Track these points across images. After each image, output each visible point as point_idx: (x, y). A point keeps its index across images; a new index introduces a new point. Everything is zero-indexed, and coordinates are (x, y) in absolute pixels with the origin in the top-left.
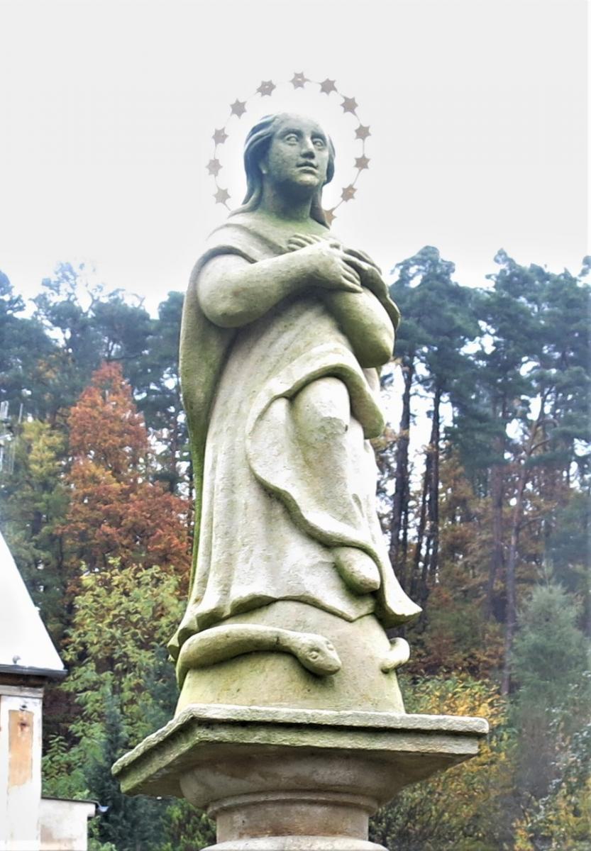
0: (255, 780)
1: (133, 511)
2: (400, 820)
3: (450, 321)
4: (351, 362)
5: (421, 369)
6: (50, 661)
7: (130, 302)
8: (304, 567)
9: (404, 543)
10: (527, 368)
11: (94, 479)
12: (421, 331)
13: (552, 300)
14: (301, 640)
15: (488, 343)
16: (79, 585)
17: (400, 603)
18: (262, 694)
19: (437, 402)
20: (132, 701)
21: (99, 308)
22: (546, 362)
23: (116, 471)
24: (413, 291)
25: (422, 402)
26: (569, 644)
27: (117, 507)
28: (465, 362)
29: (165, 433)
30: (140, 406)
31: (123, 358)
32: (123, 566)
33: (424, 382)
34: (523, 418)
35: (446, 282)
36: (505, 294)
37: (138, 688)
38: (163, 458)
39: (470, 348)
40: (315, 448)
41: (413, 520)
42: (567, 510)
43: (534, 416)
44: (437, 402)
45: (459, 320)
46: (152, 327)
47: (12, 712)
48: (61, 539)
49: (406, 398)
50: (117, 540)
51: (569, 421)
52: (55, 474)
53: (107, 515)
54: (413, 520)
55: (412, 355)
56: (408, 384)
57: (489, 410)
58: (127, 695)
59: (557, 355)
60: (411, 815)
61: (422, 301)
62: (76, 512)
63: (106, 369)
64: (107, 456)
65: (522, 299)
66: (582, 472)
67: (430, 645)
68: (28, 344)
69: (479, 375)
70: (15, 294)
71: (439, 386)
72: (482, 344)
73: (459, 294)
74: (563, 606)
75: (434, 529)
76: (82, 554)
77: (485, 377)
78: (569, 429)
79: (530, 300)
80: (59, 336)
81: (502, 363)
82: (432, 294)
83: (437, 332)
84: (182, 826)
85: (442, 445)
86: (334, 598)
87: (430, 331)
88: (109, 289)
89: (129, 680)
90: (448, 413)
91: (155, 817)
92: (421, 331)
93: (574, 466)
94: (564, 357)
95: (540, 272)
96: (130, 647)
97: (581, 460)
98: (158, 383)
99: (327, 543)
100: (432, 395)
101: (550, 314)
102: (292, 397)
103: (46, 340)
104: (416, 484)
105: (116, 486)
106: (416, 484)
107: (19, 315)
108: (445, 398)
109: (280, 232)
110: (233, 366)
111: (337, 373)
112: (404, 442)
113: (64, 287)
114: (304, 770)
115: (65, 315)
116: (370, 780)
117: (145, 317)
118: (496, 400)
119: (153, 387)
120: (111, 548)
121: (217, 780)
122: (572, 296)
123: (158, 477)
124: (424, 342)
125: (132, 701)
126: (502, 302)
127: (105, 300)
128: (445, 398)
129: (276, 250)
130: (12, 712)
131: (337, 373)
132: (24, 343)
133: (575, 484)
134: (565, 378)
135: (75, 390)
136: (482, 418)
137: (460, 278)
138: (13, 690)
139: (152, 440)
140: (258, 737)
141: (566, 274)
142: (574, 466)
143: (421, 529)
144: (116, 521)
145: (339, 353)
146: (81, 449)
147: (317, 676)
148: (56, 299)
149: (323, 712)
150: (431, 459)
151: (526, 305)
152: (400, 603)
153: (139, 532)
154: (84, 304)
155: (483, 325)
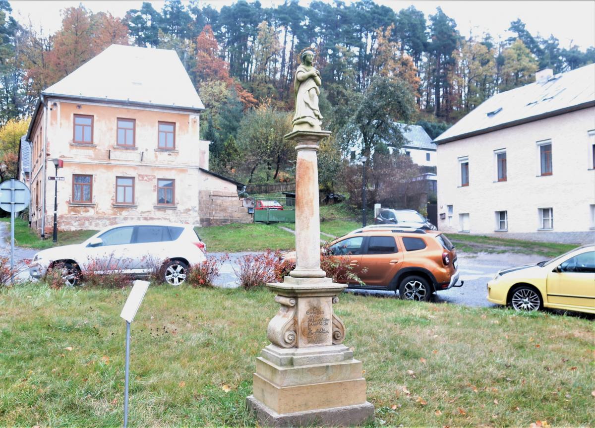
0: (304, 138)
1: (214, 65)
2: (282, 146)
3: (298, 16)
4: (315, 86)
5: (289, 29)
6: (201, 106)
7: (213, 8)
8: (311, 113)
9: (284, 76)
10: (317, 29)
11: (204, 57)
12: (290, 19)
13: (324, 11)
14: (310, 122)
15: (307, 22)
16: (200, 84)
17: (321, 117)
18: (305, 128)
19: (293, 38)
20: (214, 116)
21: (204, 9)
22: (322, 28)
23: (210, 55)
24: (288, 7)
25: (290, 37)
26: (324, 103)
27: (210, 64)
28: (302, 27)
29: (222, 44)
30: (216, 37)
31: (211, 23)
32: (211, 81)
33: (290, 32)
34: (316, 43)
35: (297, 5)
36: (312, 9)
37: (216, 112)
38: (221, 51)
39: (302, 23)
40: (311, 97)
41: (286, 70)
42: (326, 68)
43: (318, 42)
44: (293, 38)
45: (300, 16)
46: (219, 15)
47: (192, 119)
48: (195, 72)
49: (286, 36)
50: (210, 73)
51: (327, 44)
52: (193, 55)
53: (208, 67)
54: (286, 70)
55: (287, 25)
56: (286, 32)
57: (307, 41)
58: (213, 114)
59: (325, 26)
60: (285, 145)
61: (291, 10)
62: (199, 66)
63: (207, 26)
64: (207, 50)
65: (317, 10)
66: (330, 58)
67: (289, 102)
68: (186, 19)
69: (304, 31)
70: (182, 5)
71: (294, 33)
72: (305, 22)
73: (300, 8)
74: (324, 93)
75: (291, 72)
76: (200, 76)
77: (306, 31)
78: (327, 46)
79: (319, 11)
80: (194, 17)
81: (310, 28)
82: (293, 8)
83: (294, 19)
84: (227, 147)
85: (294, 50)
86: (314, 116)
87: (292, 18)
88: (207, 4)
89: (214, 110)
90: (296, 41)
91: (221, 145)
92: (290, 19)
93: (328, 57)
94: (327, 27)
95: (322, 3)
96: (213, 102)
97: (330, 55)
98: (220, 31)
99: (313, 109)
100: (292, 36)
101: (324, 15)
102: (309, 91)
103: (189, 17)
104: (287, 60)
105: (209, 59)
106: (287, 60)
107: (183, 10)
108: (295, 36)
109: (307, 68)
110: (301, 86)
111: (314, 88)
112: (284, 48)
113: (196, 3)
114: (309, 137)
115: (195, 11)
116: (317, 138)
117: (217, 12)
118: (309, 38)
119: (219, 31)
120: (208, 75)
121: (299, 138)
122: (330, 10)
123: (220, 56)
124: (290, 21)
125: (214, 116)
126: (311, 11)
127: (206, 7)
128: (295, 36)
129: (307, 71)
130: (192, 119)
131: (314, 88)
132: (185, 18)
133: (328, 61)
134: (327, 33)
135: (198, 32)
136: (305, 43)
137: (300, 4)
138: (193, 113)
139: (218, 46)
140: (305, 133)
141: (328, 4)
142: (328, 57)
143: (288, 73)
144: (210, 68)
145: (315, 85)
146: (200, 49)
147: (312, 126)
148: (193, 6)
149: (313, 131)
150: (291, 53)
151: (408, 310)
152: (321, 117)
153: (216, 72)
154: (200, 8)
155: (306, 17)
